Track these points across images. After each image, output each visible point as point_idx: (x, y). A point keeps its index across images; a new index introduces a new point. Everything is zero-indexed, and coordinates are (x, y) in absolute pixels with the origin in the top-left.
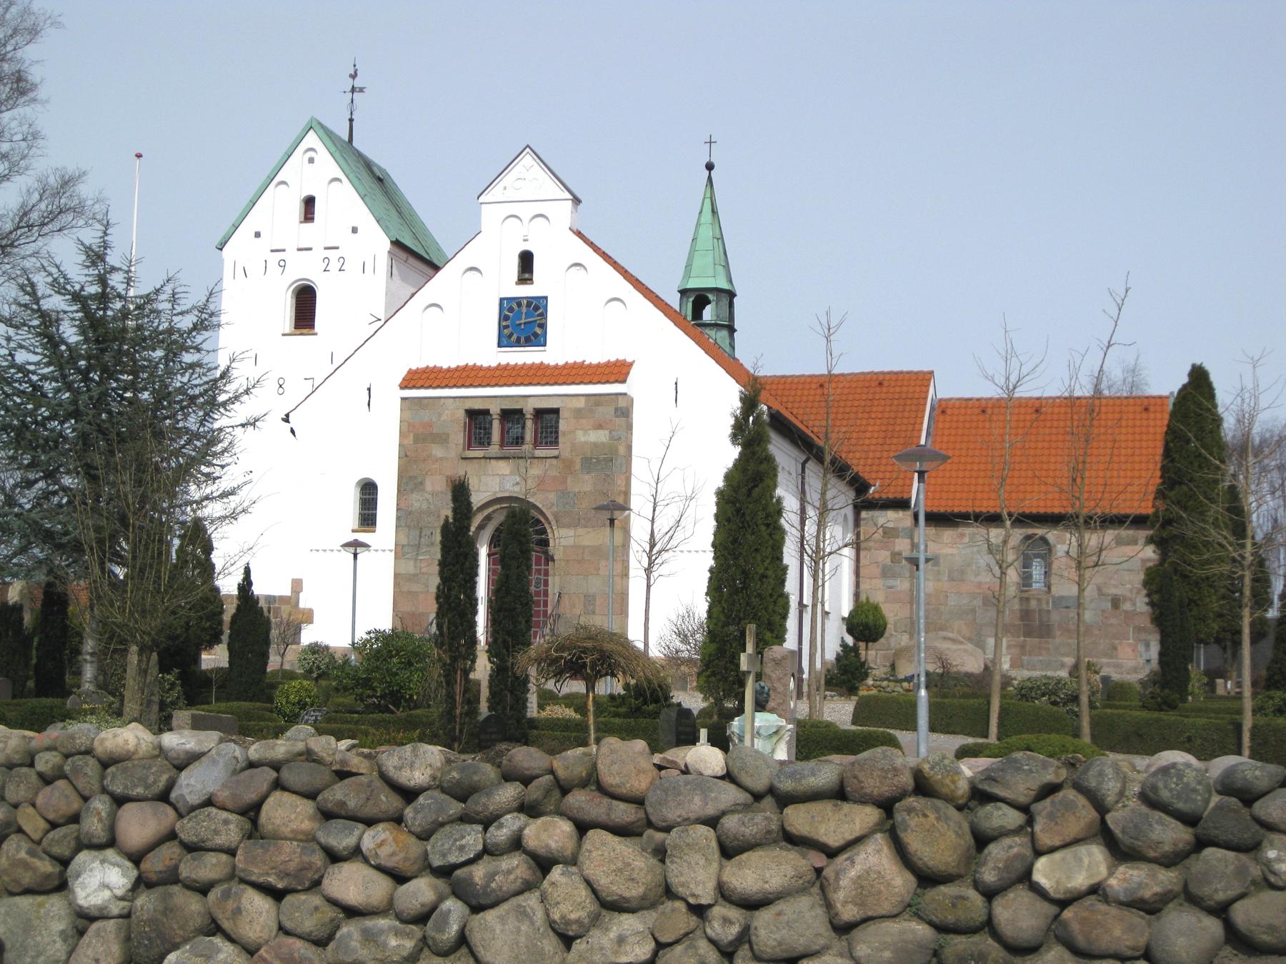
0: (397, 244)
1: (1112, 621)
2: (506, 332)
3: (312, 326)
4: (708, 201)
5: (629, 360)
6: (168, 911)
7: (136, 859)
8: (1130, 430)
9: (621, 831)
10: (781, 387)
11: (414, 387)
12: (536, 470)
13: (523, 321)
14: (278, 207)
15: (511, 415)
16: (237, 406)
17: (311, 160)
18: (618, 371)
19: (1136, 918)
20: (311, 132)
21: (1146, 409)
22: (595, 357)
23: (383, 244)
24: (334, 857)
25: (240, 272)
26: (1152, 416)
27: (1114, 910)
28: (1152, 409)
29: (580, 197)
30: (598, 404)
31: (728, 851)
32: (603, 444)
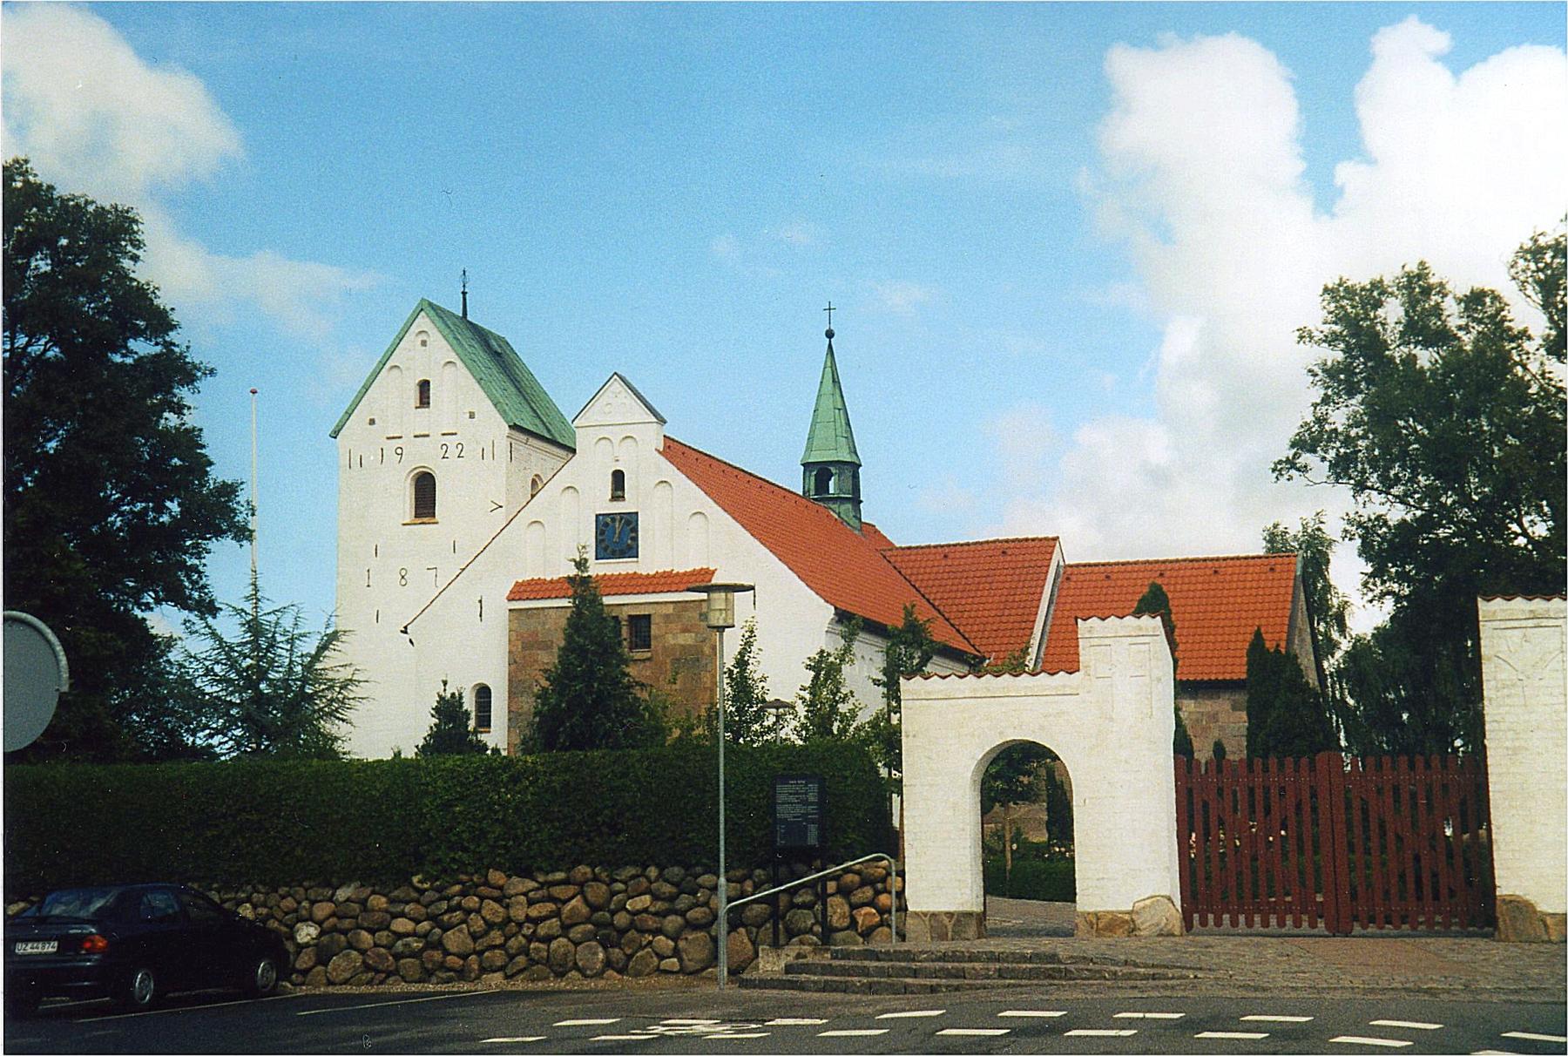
3: (433, 515)
4: (829, 370)
6: (332, 941)
7: (320, 923)
9: (495, 900)
13: (617, 535)
14: (395, 392)
17: (424, 343)
24: (395, 916)
31: (531, 903)
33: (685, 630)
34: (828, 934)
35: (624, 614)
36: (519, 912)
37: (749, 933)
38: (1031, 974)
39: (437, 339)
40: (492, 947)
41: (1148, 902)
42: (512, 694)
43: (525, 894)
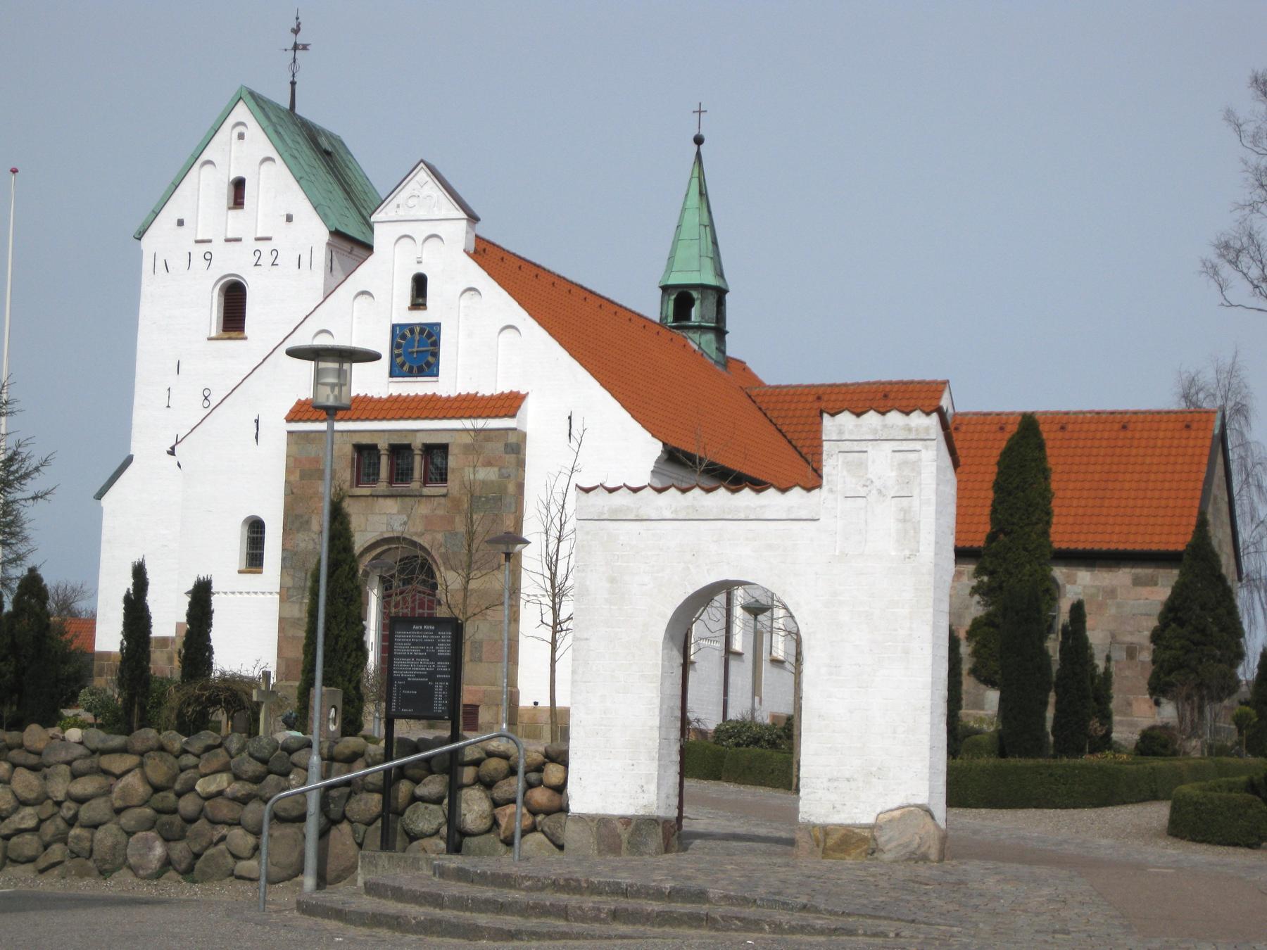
0: (336, 234)
1: (1127, 673)
2: (399, 360)
4: (695, 182)
5: (523, 392)
8: (1165, 451)
9: (33, 768)
10: (774, 399)
11: (300, 420)
12: (423, 509)
14: (203, 191)
15: (400, 451)
16: (28, 481)
17: (241, 136)
18: (510, 403)
19: (236, 806)
20: (241, 103)
21: (1188, 427)
22: (488, 389)
23: (321, 234)
25: (160, 264)
26: (1193, 434)
27: (225, 802)
28: (1194, 426)
29: (477, 211)
30: (488, 439)
31: (75, 776)
32: (492, 482)
33: (489, 464)
34: (457, 839)
35: (417, 442)
36: (59, 788)
37: (354, 831)
38: (665, 919)
39: (254, 130)
40: (20, 832)
41: (897, 813)
42: (288, 530)
43: (69, 763)
